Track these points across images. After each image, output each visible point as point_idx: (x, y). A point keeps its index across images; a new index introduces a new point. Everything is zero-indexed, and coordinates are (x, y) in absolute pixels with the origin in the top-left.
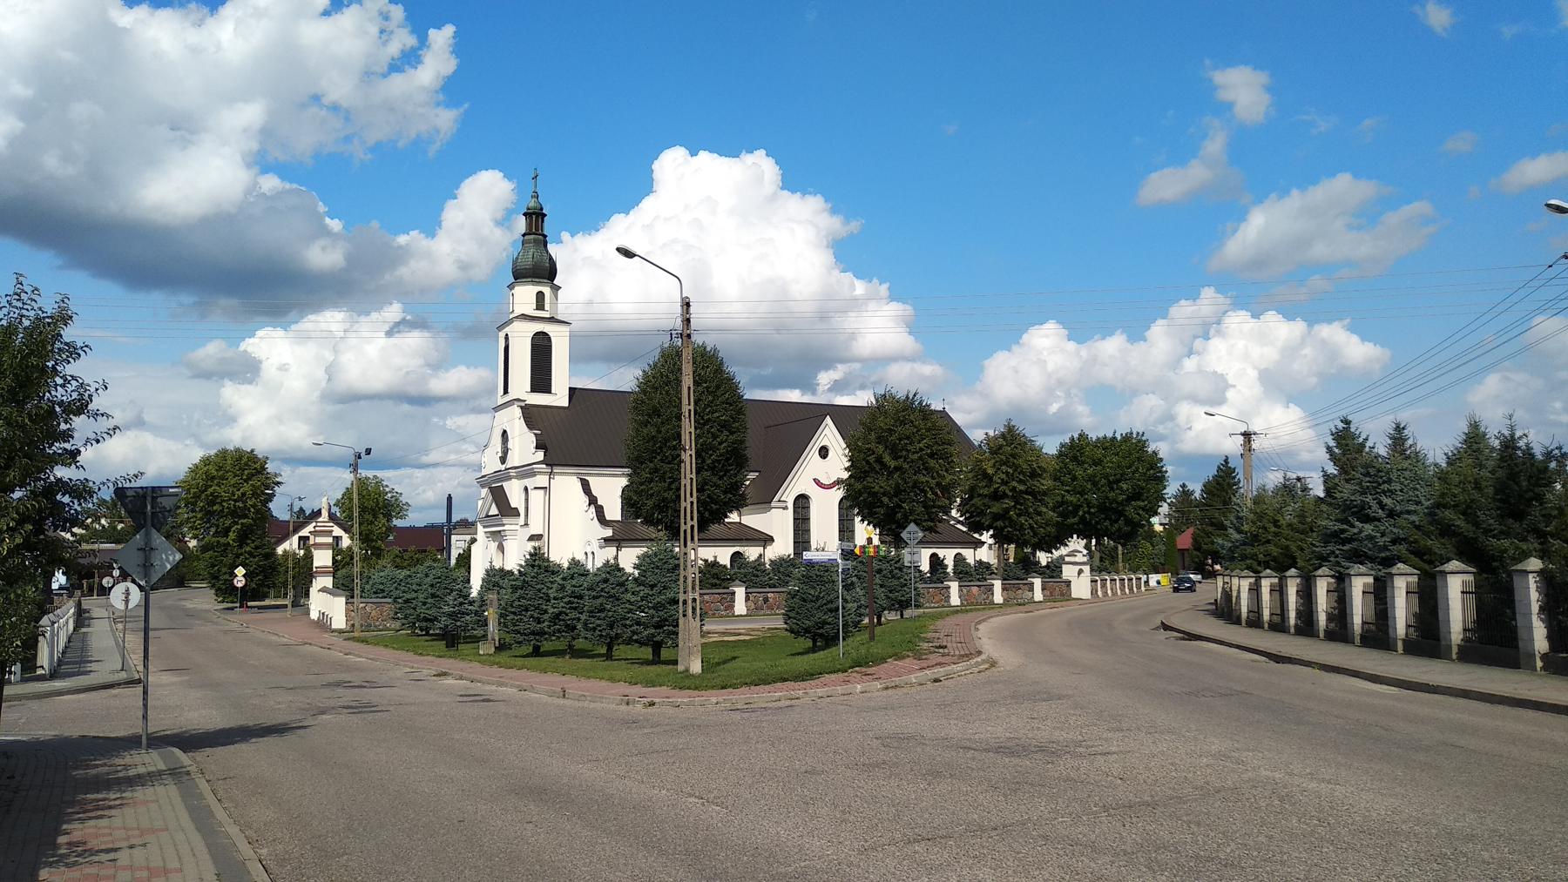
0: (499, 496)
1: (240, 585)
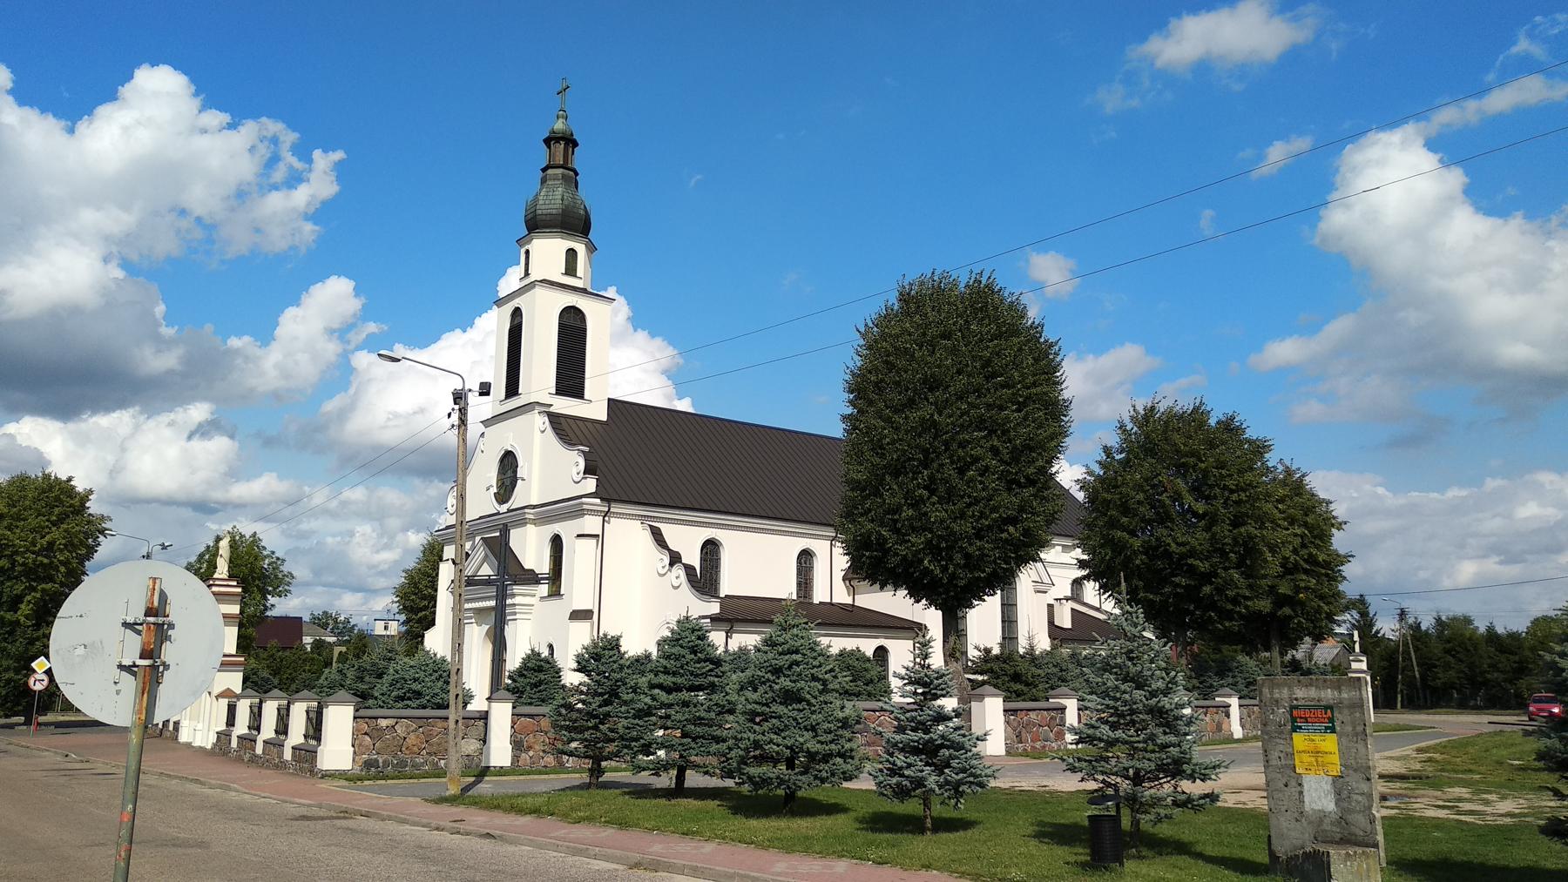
0: (500, 549)
1: (38, 687)
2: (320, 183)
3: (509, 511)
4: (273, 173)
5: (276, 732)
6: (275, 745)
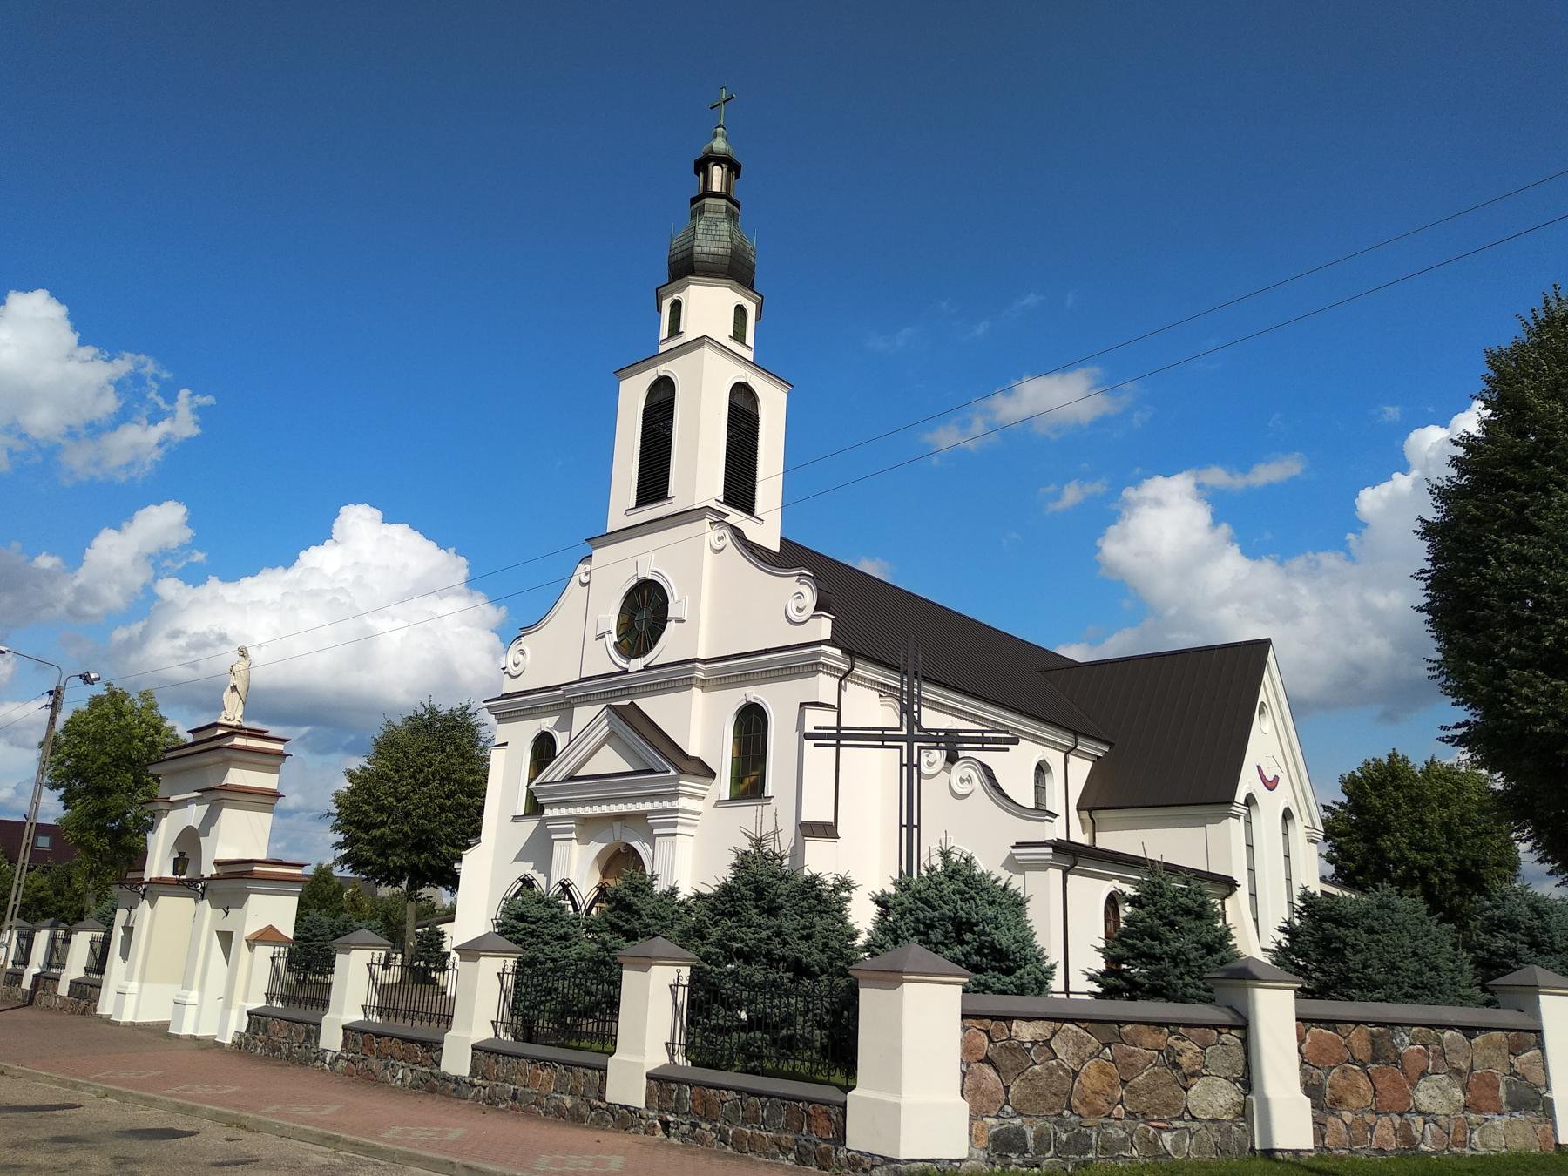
2: (183, 423)
3: (646, 668)
4: (133, 401)
5: (87, 970)
6: (45, 981)
